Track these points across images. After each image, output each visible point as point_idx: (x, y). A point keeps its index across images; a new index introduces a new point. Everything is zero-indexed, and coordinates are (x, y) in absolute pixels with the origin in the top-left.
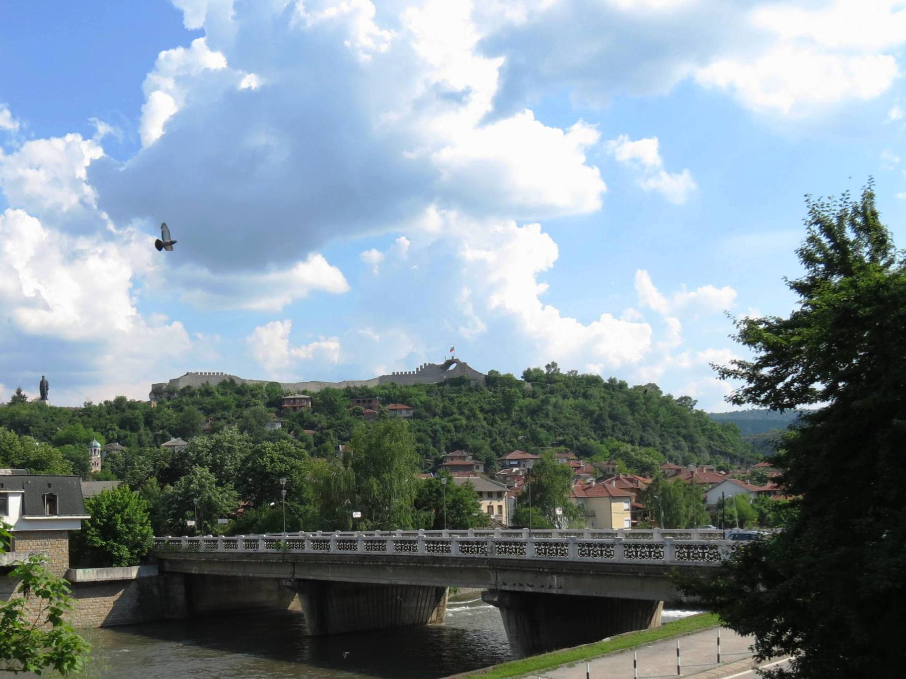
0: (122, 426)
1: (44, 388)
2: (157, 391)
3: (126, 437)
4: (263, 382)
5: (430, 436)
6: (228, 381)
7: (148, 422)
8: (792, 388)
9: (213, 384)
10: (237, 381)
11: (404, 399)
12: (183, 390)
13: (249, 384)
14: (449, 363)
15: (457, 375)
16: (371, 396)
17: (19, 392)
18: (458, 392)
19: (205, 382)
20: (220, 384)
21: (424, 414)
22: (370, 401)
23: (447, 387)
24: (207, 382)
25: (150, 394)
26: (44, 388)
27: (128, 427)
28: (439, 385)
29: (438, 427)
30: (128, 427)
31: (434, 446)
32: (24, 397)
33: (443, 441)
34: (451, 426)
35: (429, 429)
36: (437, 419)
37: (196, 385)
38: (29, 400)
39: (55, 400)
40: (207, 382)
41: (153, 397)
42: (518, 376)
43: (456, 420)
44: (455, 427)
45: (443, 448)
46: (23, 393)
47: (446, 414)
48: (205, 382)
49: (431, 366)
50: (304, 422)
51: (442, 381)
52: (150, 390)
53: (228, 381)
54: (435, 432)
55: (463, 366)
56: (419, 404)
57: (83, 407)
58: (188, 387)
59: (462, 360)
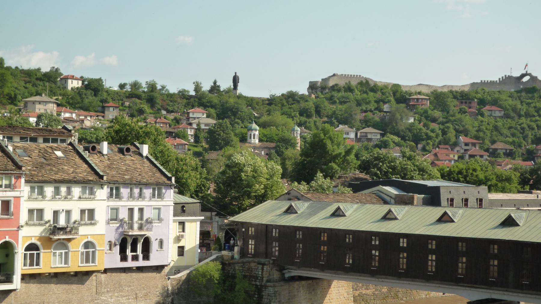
0: (301, 114)
1: (236, 80)
2: (313, 87)
3: (306, 122)
4: (389, 84)
5: (520, 133)
6: (364, 81)
7: (318, 112)
8: (207, 146)
9: (354, 83)
10: (370, 82)
11: (495, 102)
12: (333, 86)
13: (379, 84)
14: (523, 76)
15: (529, 86)
16: (469, 99)
17: (215, 83)
18: (532, 98)
19: (348, 82)
20: (359, 84)
21: (512, 114)
22: (470, 103)
23: (523, 94)
24: (349, 82)
25: (308, 89)
26: (236, 80)
27: (305, 115)
28: (518, 92)
29: (525, 126)
30: (305, 115)
31: (524, 139)
32: (219, 86)
33: (530, 136)
34: (534, 125)
35: (519, 127)
36: (523, 120)
37: (342, 83)
38: (222, 89)
39: (243, 90)
40: (349, 82)
41: (310, 91)
42: (303, 90)
43: (537, 121)
44: (537, 126)
45: (530, 141)
46: (218, 84)
47: (528, 115)
48: (348, 82)
49: (510, 77)
50: (429, 117)
51: (519, 89)
52: (308, 86)
53: (364, 81)
54: (523, 129)
55: (534, 79)
56: (508, 107)
57: (269, 97)
58: (336, 85)
59: (534, 74)
